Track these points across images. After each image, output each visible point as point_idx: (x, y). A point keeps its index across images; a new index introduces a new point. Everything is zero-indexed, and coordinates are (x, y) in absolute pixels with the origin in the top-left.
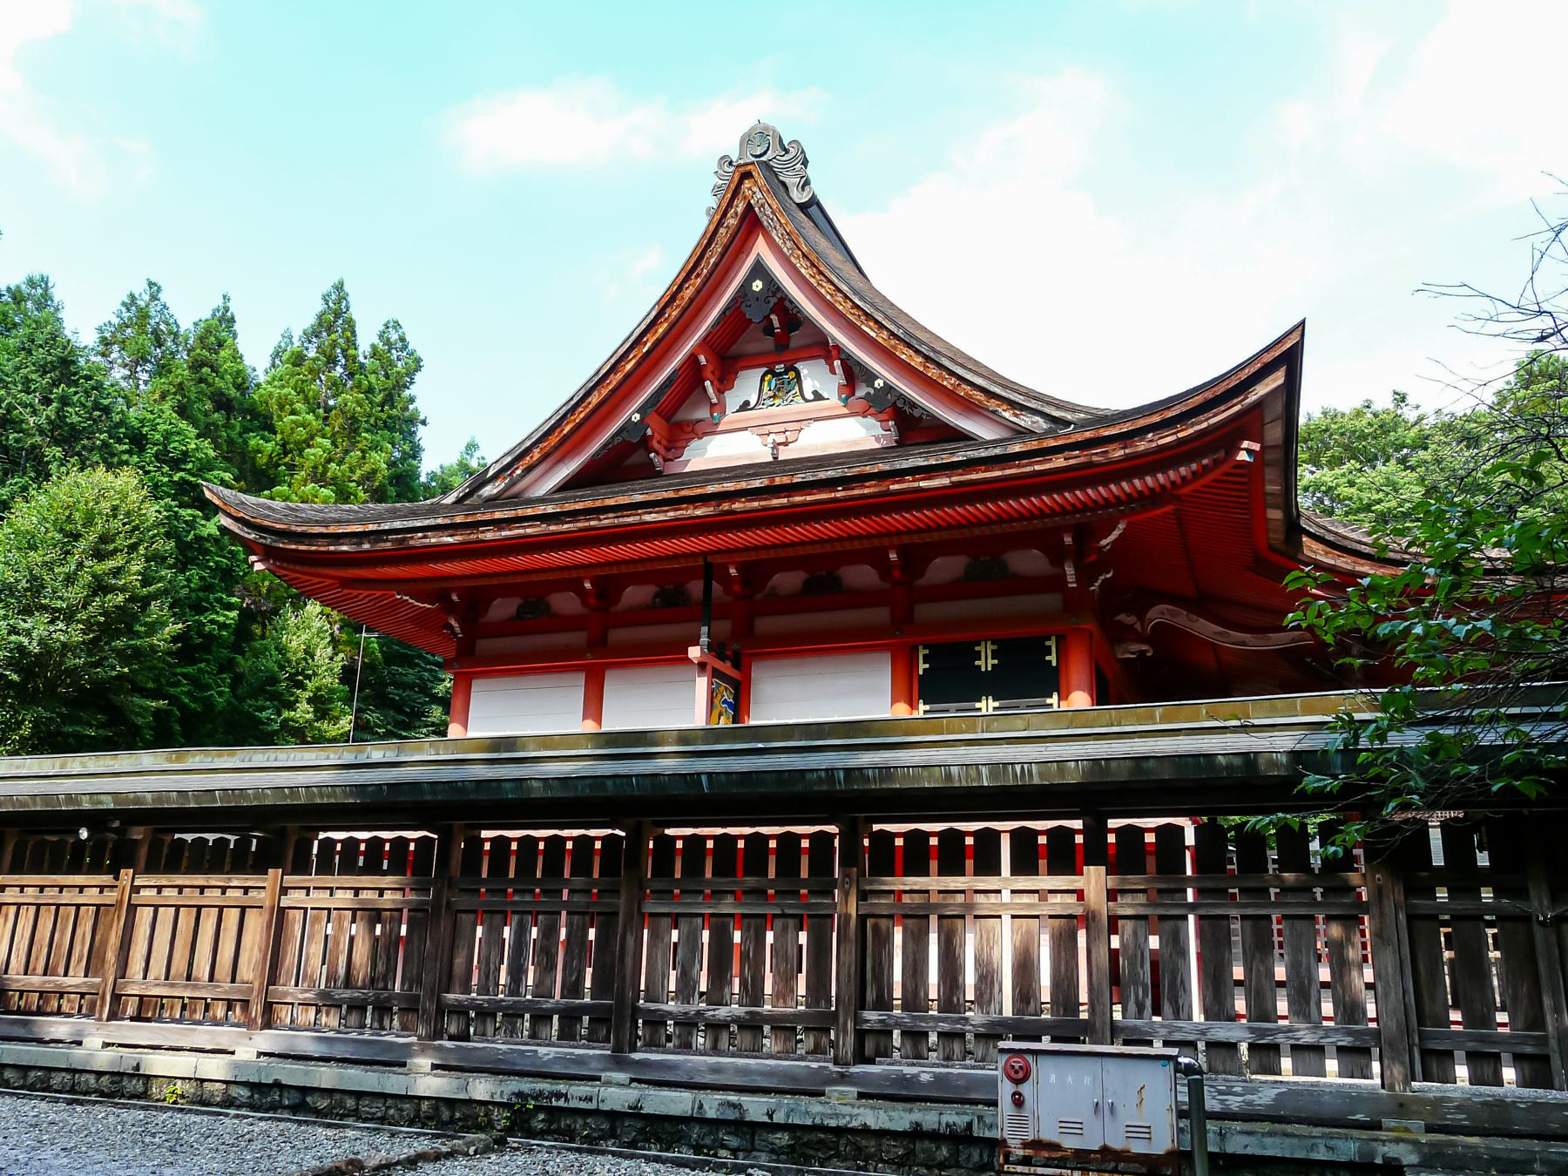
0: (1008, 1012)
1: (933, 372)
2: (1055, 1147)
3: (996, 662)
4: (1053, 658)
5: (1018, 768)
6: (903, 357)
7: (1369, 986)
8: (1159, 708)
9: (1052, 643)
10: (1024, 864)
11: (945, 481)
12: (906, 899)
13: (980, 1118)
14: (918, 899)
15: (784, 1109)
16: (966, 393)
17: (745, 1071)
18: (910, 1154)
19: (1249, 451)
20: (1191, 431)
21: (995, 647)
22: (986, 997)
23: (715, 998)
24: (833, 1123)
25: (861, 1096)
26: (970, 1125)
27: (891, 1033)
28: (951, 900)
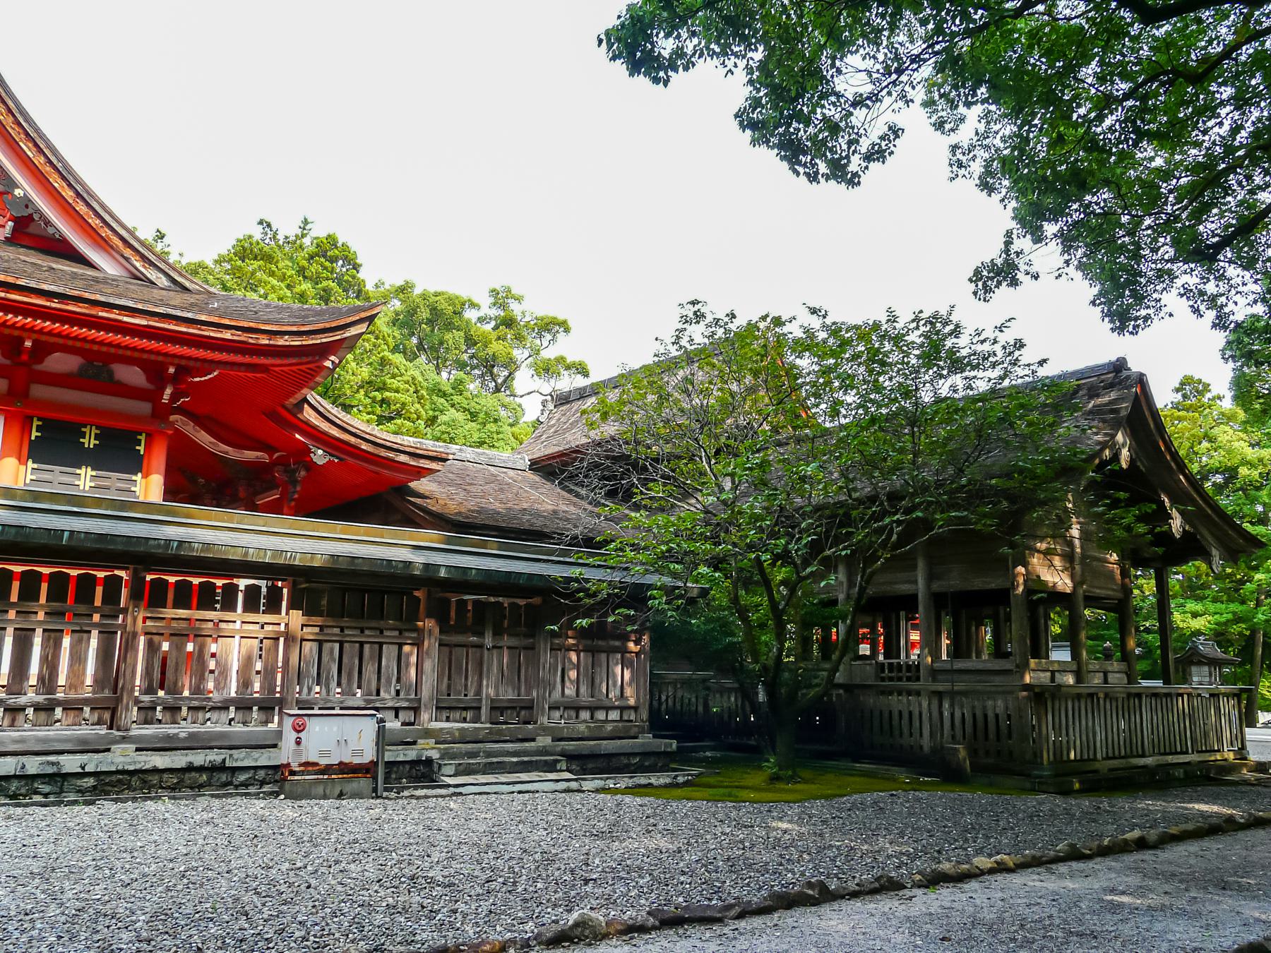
0: (233, 694)
1: (81, 208)
2: (316, 764)
3: (97, 442)
4: (141, 449)
5: (289, 554)
6: (56, 185)
7: (258, 673)
8: (341, 524)
9: (143, 438)
10: (252, 604)
11: (144, 322)
12: (174, 624)
13: (231, 756)
14: (184, 625)
15: (93, 762)
16: (107, 236)
17: (45, 740)
18: (181, 781)
19: (333, 362)
20: (311, 342)
21: (98, 432)
22: (222, 685)
23: (15, 688)
24: (131, 768)
25: (137, 750)
26: (224, 760)
27: (155, 709)
28: (204, 625)
